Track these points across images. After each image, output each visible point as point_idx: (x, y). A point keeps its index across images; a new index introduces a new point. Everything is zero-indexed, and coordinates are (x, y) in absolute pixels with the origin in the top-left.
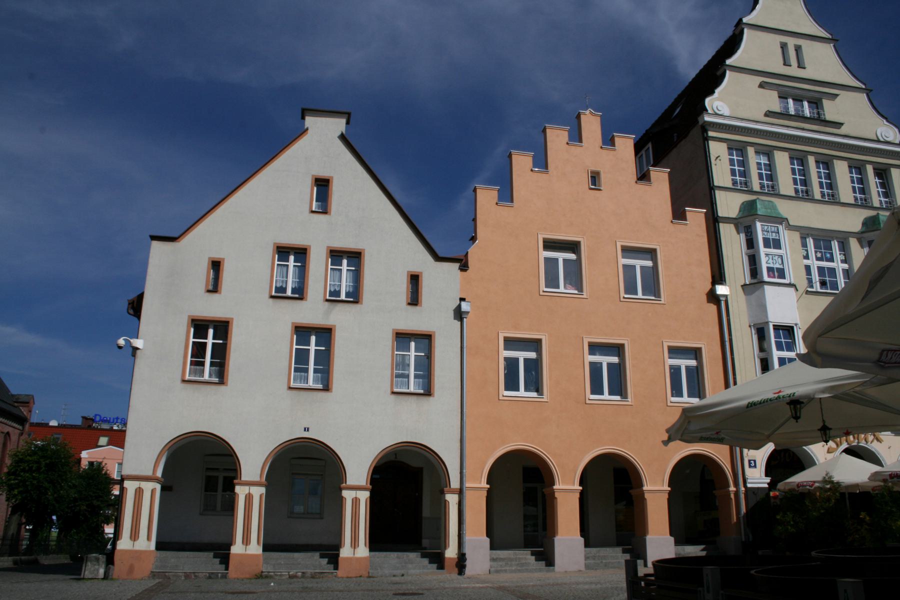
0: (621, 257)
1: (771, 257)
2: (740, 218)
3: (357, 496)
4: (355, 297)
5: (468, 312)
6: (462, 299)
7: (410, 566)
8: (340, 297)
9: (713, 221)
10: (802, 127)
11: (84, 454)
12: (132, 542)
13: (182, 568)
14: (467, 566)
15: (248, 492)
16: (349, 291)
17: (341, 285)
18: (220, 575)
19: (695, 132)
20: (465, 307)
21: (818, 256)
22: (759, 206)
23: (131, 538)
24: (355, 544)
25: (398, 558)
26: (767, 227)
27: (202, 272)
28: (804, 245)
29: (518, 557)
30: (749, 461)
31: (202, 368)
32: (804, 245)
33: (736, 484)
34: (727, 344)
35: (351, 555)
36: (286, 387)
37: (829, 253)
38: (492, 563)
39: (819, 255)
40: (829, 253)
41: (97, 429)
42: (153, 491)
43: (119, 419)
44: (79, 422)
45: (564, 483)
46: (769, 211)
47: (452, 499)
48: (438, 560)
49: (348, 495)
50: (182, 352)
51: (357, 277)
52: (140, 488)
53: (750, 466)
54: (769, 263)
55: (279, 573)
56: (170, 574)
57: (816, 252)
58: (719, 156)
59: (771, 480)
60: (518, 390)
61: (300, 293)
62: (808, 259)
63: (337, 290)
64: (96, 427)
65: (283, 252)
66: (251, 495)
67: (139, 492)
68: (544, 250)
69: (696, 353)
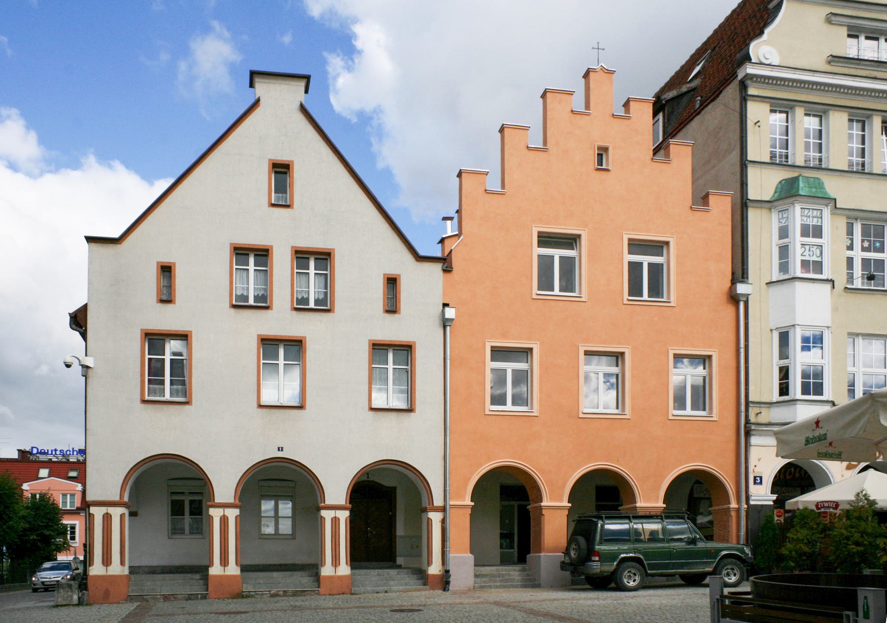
0: (627, 252)
1: (807, 247)
2: (774, 201)
3: (337, 516)
4: (325, 306)
5: (452, 320)
6: (445, 305)
7: (392, 583)
8: (309, 305)
9: (743, 205)
10: (874, 76)
11: (25, 486)
12: (105, 568)
13: (159, 590)
14: (451, 582)
15: (223, 514)
16: (318, 298)
17: (309, 291)
18: (199, 596)
19: (731, 92)
20: (450, 313)
21: (865, 246)
22: (801, 184)
23: (103, 563)
24: (336, 562)
25: (379, 575)
26: (808, 210)
27: (151, 278)
28: (850, 232)
29: (501, 573)
30: (755, 478)
31: (162, 387)
32: (850, 232)
33: (739, 501)
34: (742, 351)
35: (333, 574)
36: (255, 405)
37: (879, 242)
38: (476, 579)
39: (866, 244)
40: (879, 242)
41: (36, 462)
42: (122, 516)
43: (57, 450)
44: (15, 455)
45: (551, 500)
46: (814, 190)
47: (435, 517)
48: (421, 574)
49: (327, 515)
50: (138, 370)
51: (328, 281)
52: (107, 513)
53: (755, 483)
54: (805, 256)
55: (260, 593)
56: (148, 597)
57: (863, 241)
58: (759, 121)
59: (777, 497)
60: (505, 404)
61: (263, 303)
62: (852, 249)
63: (305, 297)
64: (34, 459)
65: (241, 252)
66: (226, 518)
67: (107, 518)
68: (538, 247)
69: (705, 360)
